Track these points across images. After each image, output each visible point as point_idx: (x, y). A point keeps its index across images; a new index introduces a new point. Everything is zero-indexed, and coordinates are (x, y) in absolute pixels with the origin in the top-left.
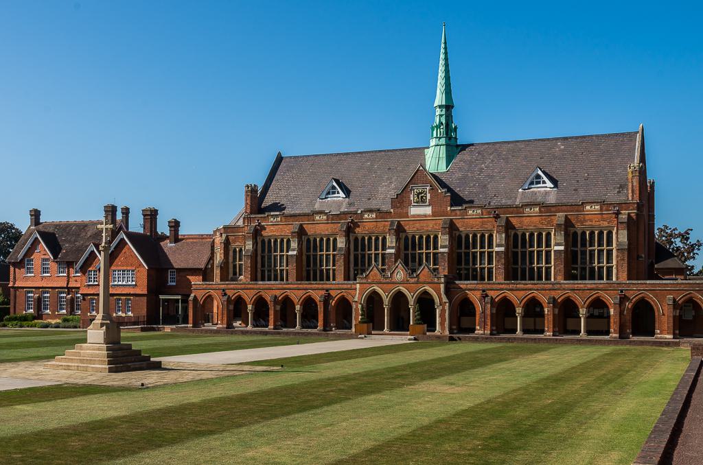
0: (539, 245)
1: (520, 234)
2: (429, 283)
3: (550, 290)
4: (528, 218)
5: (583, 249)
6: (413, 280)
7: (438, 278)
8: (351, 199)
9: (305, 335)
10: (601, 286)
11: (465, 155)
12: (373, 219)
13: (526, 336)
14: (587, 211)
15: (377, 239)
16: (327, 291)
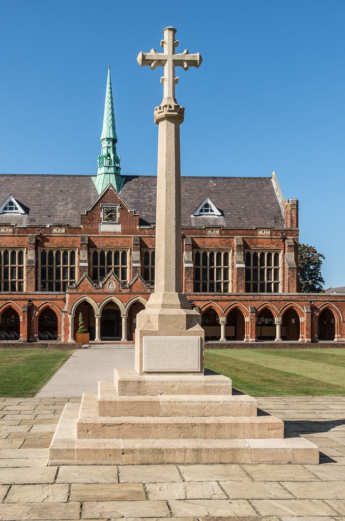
0: (13, 262)
1: (99, 252)
2: (142, 294)
3: (251, 301)
4: (209, 239)
5: (255, 267)
6: (125, 291)
7: (151, 289)
8: (31, 216)
9: (16, 347)
10: (294, 297)
11: (131, 184)
12: (62, 233)
13: (229, 342)
14: (260, 235)
15: (65, 254)
16: (30, 301)
